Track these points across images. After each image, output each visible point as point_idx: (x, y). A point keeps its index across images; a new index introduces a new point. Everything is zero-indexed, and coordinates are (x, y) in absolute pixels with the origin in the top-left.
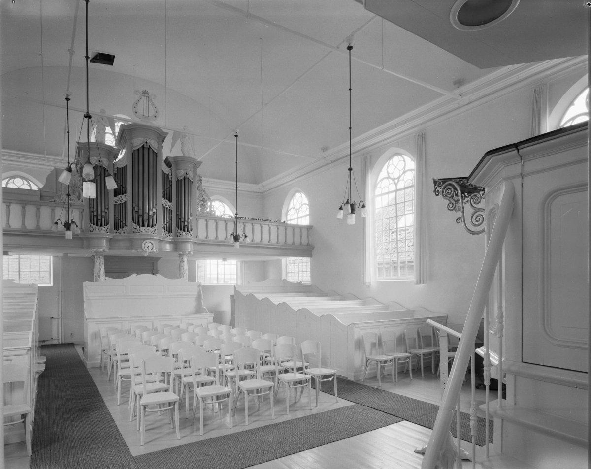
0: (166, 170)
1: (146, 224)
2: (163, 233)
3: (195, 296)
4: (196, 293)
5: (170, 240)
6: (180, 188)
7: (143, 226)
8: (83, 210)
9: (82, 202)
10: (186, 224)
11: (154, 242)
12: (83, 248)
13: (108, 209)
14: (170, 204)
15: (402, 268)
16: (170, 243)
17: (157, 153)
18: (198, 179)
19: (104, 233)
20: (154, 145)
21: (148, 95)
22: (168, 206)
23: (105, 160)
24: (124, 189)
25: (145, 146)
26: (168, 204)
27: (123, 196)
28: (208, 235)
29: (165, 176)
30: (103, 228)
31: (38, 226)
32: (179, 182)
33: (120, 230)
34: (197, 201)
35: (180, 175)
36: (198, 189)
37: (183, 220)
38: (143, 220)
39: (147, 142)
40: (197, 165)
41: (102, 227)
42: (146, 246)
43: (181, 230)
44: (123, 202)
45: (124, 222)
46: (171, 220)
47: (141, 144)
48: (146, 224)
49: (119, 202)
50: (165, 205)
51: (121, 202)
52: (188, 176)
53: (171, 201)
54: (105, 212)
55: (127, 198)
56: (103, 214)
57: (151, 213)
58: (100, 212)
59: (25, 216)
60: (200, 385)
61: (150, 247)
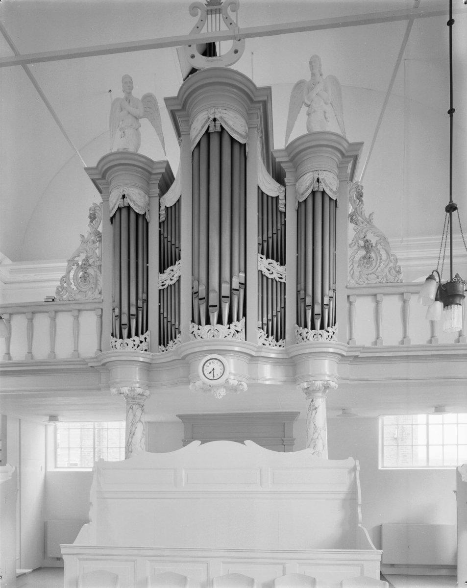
0: (271, 188)
1: (214, 317)
2: (259, 336)
3: (342, 496)
4: (344, 489)
5: (273, 355)
6: (301, 226)
7: (208, 322)
8: (320, 334)
9: (100, 293)
10: (318, 309)
11: (234, 363)
12: (99, 389)
14: (281, 269)
15: (118, 390)
16: (276, 362)
17: (336, 200)
18: (354, 194)
19: (132, 351)
20: (236, 125)
21: (217, 7)
24: (177, 250)
25: (211, 130)
26: (275, 270)
28: (382, 335)
29: (268, 204)
30: (130, 341)
31: (30, 353)
32: (302, 206)
33: (171, 343)
34: (350, 252)
35: (302, 190)
36: (352, 220)
37: (309, 301)
38: (215, 309)
39: (215, 120)
40: (349, 157)
42: (208, 368)
44: (175, 279)
45: (162, 236)
46: (285, 307)
47: (203, 127)
48: (214, 317)
50: (267, 273)
51: (172, 283)
52: (322, 186)
53: (283, 263)
55: (182, 269)
58: (125, 309)
59: (32, 338)
61: (218, 372)
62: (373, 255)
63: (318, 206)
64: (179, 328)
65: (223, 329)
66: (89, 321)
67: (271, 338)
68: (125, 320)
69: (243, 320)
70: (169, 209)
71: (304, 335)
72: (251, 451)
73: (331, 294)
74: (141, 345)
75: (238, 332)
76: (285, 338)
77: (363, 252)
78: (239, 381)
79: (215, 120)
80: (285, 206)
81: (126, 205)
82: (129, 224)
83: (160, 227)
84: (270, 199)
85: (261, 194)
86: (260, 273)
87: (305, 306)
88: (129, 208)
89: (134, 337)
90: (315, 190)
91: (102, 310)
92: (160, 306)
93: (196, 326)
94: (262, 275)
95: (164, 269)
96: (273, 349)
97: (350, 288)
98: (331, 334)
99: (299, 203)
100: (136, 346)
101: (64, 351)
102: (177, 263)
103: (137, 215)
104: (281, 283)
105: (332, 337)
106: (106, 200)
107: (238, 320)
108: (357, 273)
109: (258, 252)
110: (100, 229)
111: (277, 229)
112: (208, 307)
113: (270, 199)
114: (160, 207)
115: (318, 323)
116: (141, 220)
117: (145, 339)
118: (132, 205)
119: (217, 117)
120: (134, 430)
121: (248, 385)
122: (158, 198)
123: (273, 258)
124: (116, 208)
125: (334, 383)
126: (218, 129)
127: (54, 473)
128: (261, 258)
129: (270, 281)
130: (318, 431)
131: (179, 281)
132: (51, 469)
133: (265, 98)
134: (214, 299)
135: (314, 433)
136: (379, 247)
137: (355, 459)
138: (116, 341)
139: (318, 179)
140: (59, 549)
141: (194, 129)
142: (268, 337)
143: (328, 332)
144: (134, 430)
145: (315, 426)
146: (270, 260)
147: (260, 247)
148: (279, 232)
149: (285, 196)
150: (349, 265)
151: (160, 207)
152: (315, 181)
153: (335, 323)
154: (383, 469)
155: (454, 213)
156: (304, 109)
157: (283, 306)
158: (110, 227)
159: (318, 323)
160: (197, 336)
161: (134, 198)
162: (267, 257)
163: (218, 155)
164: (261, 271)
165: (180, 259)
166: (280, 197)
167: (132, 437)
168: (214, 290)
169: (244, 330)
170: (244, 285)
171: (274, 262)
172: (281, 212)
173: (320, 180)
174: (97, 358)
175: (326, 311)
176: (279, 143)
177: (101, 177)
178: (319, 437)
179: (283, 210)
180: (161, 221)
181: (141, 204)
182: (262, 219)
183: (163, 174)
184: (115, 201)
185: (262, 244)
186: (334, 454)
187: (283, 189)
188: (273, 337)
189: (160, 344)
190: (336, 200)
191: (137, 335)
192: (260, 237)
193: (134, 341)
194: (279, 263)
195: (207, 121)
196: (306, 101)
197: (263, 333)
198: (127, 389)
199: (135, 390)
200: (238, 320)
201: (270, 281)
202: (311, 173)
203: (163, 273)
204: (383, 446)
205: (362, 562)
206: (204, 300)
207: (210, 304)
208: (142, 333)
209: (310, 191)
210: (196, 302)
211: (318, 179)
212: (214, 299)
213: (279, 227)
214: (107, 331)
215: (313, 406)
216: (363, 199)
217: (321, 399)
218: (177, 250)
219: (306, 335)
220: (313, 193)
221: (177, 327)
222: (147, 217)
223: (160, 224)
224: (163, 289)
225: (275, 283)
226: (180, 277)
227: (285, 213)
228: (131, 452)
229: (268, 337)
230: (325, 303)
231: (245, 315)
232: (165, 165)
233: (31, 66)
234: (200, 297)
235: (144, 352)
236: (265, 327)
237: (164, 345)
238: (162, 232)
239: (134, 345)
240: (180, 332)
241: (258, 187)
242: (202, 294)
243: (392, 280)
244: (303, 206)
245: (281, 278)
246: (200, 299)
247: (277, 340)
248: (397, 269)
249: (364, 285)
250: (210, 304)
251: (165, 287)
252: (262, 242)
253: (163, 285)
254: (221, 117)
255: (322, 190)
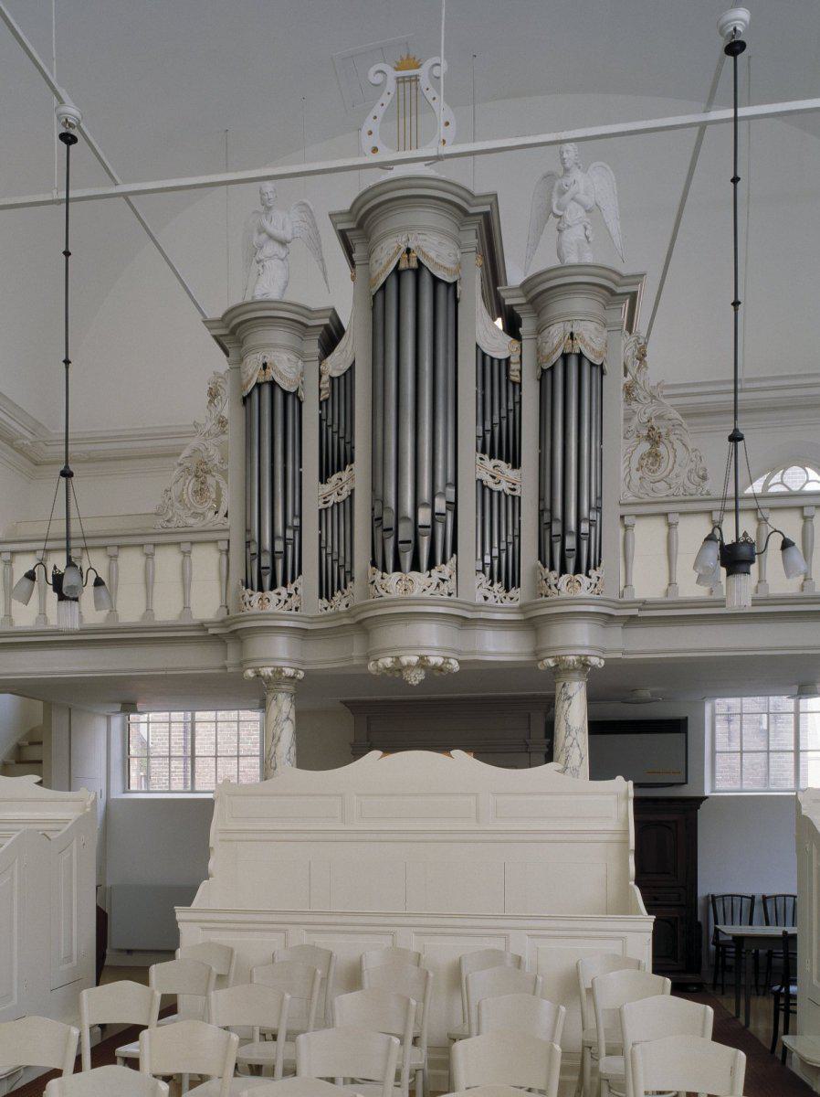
1: (407, 560)
2: (478, 590)
7: (397, 568)
10: (571, 542)
13: (599, 509)
22: (504, 487)
23: (591, 326)
24: (348, 447)
25: (402, 266)
26: (503, 476)
27: (345, 475)
29: (495, 374)
30: (272, 595)
32: (545, 376)
33: (338, 594)
35: (547, 351)
37: (557, 529)
39: (408, 251)
41: (577, 577)
43: (552, 568)
44: (345, 494)
45: (348, 568)
48: (407, 560)
49: (333, 499)
50: (490, 483)
51: (340, 499)
52: (579, 346)
53: (516, 463)
54: (592, 523)
55: (357, 476)
56: (279, 546)
57: (424, 516)
60: (349, 1081)
62: (662, 449)
63: (569, 376)
64: (351, 572)
65: (420, 579)
66: (206, 561)
67: (496, 586)
68: (266, 561)
69: (452, 562)
70: (336, 381)
71: (552, 581)
72: (460, 768)
73: (593, 516)
74: (289, 600)
75: (443, 580)
76: (519, 586)
77: (645, 447)
78: (444, 658)
79: (408, 251)
80: (521, 372)
81: (268, 379)
82: (268, 406)
83: (321, 408)
84: (496, 362)
85: (482, 356)
86: (479, 482)
87: (551, 536)
88: (273, 384)
89: (280, 589)
90: (568, 351)
91: (229, 541)
92: (320, 536)
93: (379, 574)
94: (484, 487)
95: (328, 476)
96: (504, 604)
97: (624, 505)
98: (594, 580)
99: (543, 371)
100: (283, 602)
101: (167, 611)
102: (348, 468)
103: (286, 394)
104: (513, 497)
105: (596, 585)
106: (238, 364)
107: (444, 562)
108: (636, 481)
109: (477, 451)
110: (226, 414)
111: (508, 411)
112: (397, 542)
113: (496, 362)
114: (320, 376)
115: (571, 564)
116: (292, 399)
117: (296, 589)
118: (277, 379)
119: (412, 246)
120: (279, 731)
121: (460, 662)
122: (317, 363)
123: (500, 458)
124: (253, 383)
125: (598, 659)
126: (414, 264)
127: (123, 800)
128: (481, 459)
129: (496, 495)
130: (573, 733)
131: (351, 497)
132: (117, 794)
133: (487, 208)
134: (405, 532)
135: (566, 738)
136: (672, 438)
137: (627, 780)
138: (251, 595)
139: (572, 334)
140: (174, 914)
141: (377, 261)
142: (492, 585)
143: (590, 577)
144: (279, 731)
145: (568, 727)
146: (496, 462)
147: (480, 442)
148: (511, 414)
149: (521, 356)
150: (622, 468)
151: (320, 376)
152: (566, 339)
153: (600, 561)
154: (714, 794)
155: (740, 444)
156: (553, 221)
157: (516, 533)
158: (240, 410)
159: (571, 564)
160: (379, 587)
161: (281, 368)
162: (492, 457)
163: (407, 298)
164: (482, 481)
165: (352, 462)
166: (512, 359)
167: (276, 745)
168: (406, 518)
169: (454, 577)
170: (453, 506)
171: (502, 464)
172: (514, 383)
173: (575, 336)
174: (223, 621)
175: (585, 544)
176: (515, 274)
177: (234, 332)
178: (575, 744)
179: (517, 379)
180: (322, 399)
181: (291, 376)
182: (484, 396)
183: (326, 326)
184: (252, 373)
185: (484, 436)
186: (600, 770)
187: (516, 344)
188: (500, 585)
189: (321, 597)
190: (602, 365)
191: (285, 584)
192: (481, 428)
193: (279, 594)
194: (510, 465)
195: (396, 253)
196: (555, 210)
197: (484, 578)
198: (270, 670)
199: (282, 671)
200: (444, 562)
201: (496, 495)
202: (562, 324)
203: (326, 482)
204: (714, 752)
205: (624, 934)
206: (391, 532)
207: (400, 539)
208: (293, 581)
209: (559, 353)
210: (379, 533)
211: (572, 334)
212: (405, 532)
213: (511, 407)
214: (237, 574)
215: (566, 694)
216: (646, 359)
217: (577, 683)
218: (348, 447)
219: (555, 582)
220: (565, 357)
221: (341, 563)
222: (301, 393)
223: (321, 403)
224: (326, 509)
225: (503, 497)
226: (352, 491)
227: (520, 384)
228: (275, 769)
229: (492, 585)
230: (582, 531)
231: (455, 550)
232: (329, 313)
233: (131, 198)
234: (386, 525)
235: (293, 612)
236: (488, 569)
237: (327, 598)
238: (324, 417)
239: (280, 601)
240: (352, 579)
241: (477, 346)
242: (389, 520)
243: (694, 491)
244: (549, 375)
245: (514, 490)
246: (384, 530)
247: (507, 590)
248: (701, 473)
249: (647, 499)
250: (400, 539)
251: (330, 504)
252: (484, 434)
253: (325, 503)
254: (419, 247)
255: (578, 351)
